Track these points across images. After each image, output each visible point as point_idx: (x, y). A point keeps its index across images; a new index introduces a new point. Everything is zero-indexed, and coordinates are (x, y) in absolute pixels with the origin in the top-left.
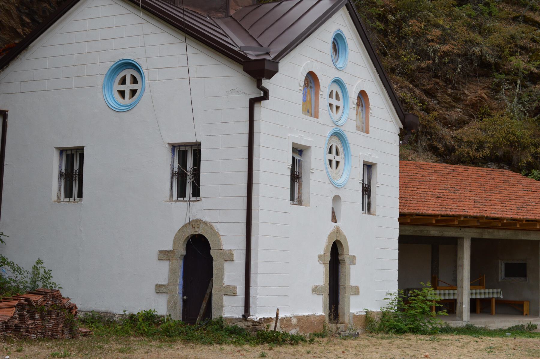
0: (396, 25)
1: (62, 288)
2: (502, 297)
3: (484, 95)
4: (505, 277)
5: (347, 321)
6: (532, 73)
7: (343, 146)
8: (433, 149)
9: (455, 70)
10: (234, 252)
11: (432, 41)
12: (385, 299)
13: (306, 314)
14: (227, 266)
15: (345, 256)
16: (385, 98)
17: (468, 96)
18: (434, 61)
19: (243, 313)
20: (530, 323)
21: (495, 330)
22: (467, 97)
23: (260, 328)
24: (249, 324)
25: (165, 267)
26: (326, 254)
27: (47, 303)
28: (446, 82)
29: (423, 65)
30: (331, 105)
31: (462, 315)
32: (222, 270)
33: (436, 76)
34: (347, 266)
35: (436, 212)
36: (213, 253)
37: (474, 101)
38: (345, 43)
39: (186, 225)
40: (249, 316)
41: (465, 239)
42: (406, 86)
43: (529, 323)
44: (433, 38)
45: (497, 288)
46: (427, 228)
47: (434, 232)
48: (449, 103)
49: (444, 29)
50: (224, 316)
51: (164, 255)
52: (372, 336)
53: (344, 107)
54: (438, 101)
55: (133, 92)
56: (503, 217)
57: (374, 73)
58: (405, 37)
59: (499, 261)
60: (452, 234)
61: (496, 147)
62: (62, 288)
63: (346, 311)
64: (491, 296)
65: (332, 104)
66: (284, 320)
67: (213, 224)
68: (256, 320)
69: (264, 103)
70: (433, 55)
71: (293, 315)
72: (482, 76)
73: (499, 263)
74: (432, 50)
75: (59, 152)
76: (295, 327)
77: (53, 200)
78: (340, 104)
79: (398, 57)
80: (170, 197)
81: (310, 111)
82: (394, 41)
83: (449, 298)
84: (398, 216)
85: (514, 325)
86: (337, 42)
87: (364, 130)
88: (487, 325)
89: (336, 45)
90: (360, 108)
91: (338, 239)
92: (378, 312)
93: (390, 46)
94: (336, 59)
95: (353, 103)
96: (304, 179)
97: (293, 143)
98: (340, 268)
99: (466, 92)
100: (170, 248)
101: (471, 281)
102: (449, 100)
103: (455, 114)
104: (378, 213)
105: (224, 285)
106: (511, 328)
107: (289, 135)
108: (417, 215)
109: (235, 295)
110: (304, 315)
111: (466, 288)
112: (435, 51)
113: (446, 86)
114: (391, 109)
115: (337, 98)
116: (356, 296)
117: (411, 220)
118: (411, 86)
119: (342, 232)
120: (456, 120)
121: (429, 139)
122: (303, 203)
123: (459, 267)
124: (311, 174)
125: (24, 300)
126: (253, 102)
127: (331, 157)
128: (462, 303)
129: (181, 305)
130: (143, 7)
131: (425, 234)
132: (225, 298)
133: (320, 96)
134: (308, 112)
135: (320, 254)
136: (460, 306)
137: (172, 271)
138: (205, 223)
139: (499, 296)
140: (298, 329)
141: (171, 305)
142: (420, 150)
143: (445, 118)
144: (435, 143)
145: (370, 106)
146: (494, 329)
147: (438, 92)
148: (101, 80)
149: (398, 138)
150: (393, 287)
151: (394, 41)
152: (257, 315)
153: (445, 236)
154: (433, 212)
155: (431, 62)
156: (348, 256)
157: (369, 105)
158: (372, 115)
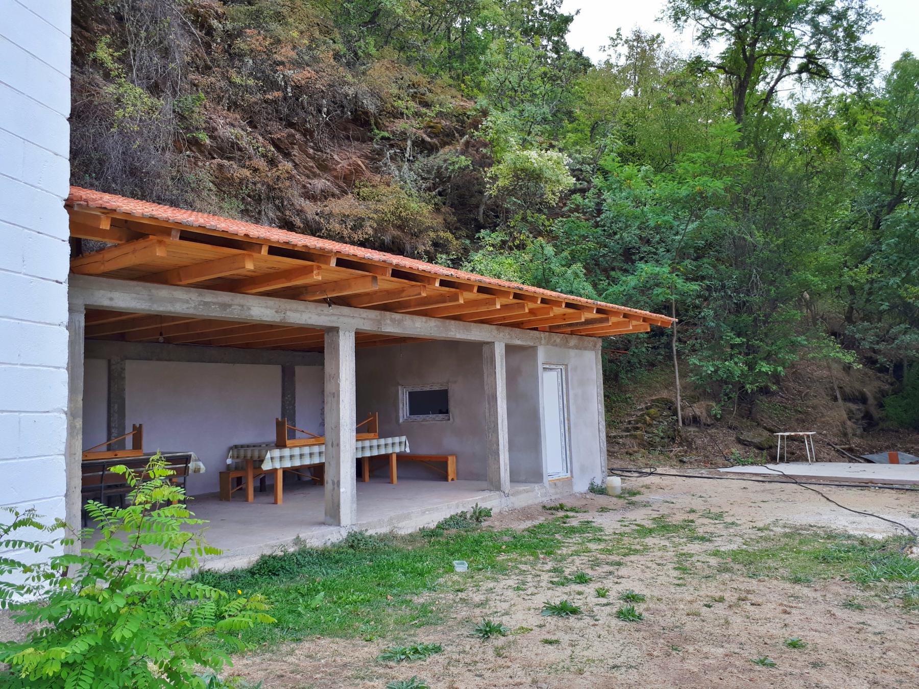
2: (408, 450)
3: (360, 163)
4: (410, 414)
6: (423, 140)
17: (339, 163)
20: (477, 505)
21: (411, 535)
22: (336, 165)
28: (305, 136)
31: (339, 512)
37: (348, 172)
41: (341, 333)
43: (474, 506)
45: (400, 435)
54: (295, 162)
56: (433, 271)
58: (241, 56)
59: (400, 388)
60: (310, 318)
61: (380, 228)
64: (390, 451)
70: (283, 84)
72: (358, 140)
73: (400, 392)
74: (282, 76)
83: (312, 463)
85: (448, 516)
88: (396, 525)
99: (336, 157)
101: (358, 422)
102: (311, 164)
103: (320, 184)
106: (442, 524)
111: (348, 447)
120: (322, 191)
121: (278, 208)
123: (328, 399)
128: (339, 482)
136: (334, 489)
139: (403, 450)
146: (410, 531)
147: (293, 148)
157: (392, 537)
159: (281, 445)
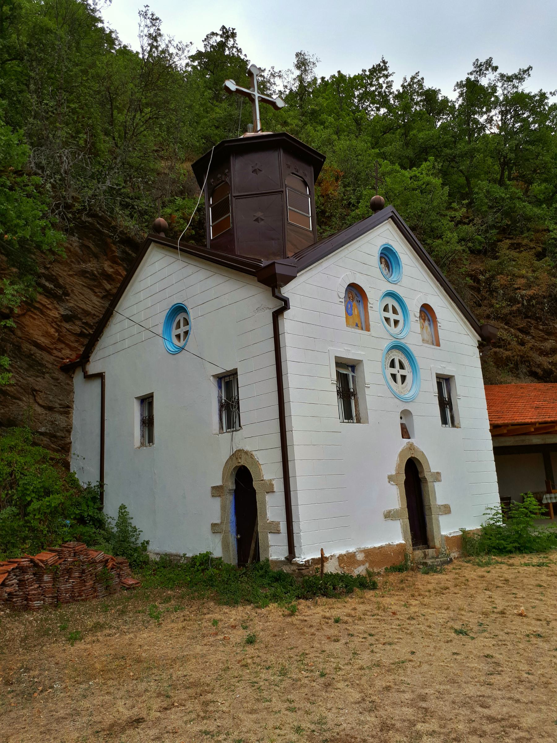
0: (486, 283)
1: (142, 531)
5: (437, 543)
7: (408, 359)
8: (533, 375)
9: (542, 310)
10: (274, 482)
11: (519, 288)
12: (484, 514)
13: (377, 545)
14: (268, 498)
15: (425, 473)
16: (456, 312)
18: (523, 304)
19: (287, 554)
23: (309, 572)
24: (294, 568)
25: (217, 503)
26: (398, 473)
27: (65, 561)
28: (537, 320)
29: (514, 308)
30: (387, 320)
32: (264, 503)
33: (527, 317)
34: (429, 484)
35: (533, 420)
36: (255, 485)
38: (397, 257)
39: (231, 457)
40: (294, 557)
42: (501, 327)
44: (519, 286)
46: (528, 437)
47: (536, 440)
48: (542, 336)
49: (528, 279)
50: (270, 558)
51: (217, 491)
52: (468, 562)
53: (404, 321)
55: (186, 333)
57: (437, 287)
58: (496, 290)
62: (142, 531)
63: (435, 533)
65: (389, 318)
66: (345, 557)
67: (254, 453)
68: (301, 563)
69: (287, 314)
71: (360, 548)
75: (140, 402)
76: (362, 563)
77: (136, 447)
78: (400, 317)
79: (492, 306)
80: (220, 429)
81: (359, 325)
82: (487, 295)
84: (489, 427)
86: (386, 255)
87: (435, 343)
89: (389, 263)
90: (427, 323)
91: (413, 456)
92: (478, 530)
93: (484, 298)
94: (389, 275)
95: (415, 316)
96: (359, 395)
97: (336, 357)
98: (422, 486)
100: (219, 483)
104: (462, 425)
105: (268, 521)
107: (330, 348)
108: (513, 425)
109: (278, 532)
110: (375, 548)
112: (522, 296)
113: (537, 324)
114: (465, 323)
115: (395, 311)
116: (447, 515)
117: (508, 431)
118: (506, 327)
119: (418, 448)
120: (551, 349)
121: (528, 366)
122: (361, 421)
124: (366, 389)
125: (28, 561)
126: (277, 315)
127: (394, 371)
129: (235, 546)
130: (181, 250)
131: (527, 443)
132: (270, 536)
133: (369, 308)
134: (357, 325)
135: (390, 474)
137: (223, 508)
138: (246, 453)
140: (367, 565)
141: (225, 545)
142: (522, 376)
143: (540, 349)
144: (533, 369)
145: (438, 320)
148: (160, 329)
149: (477, 351)
150: (495, 501)
151: (487, 295)
152: (303, 557)
153: (549, 442)
154: (530, 421)
155: (520, 305)
156: (429, 473)
158: (442, 328)
159: (549, 492)
